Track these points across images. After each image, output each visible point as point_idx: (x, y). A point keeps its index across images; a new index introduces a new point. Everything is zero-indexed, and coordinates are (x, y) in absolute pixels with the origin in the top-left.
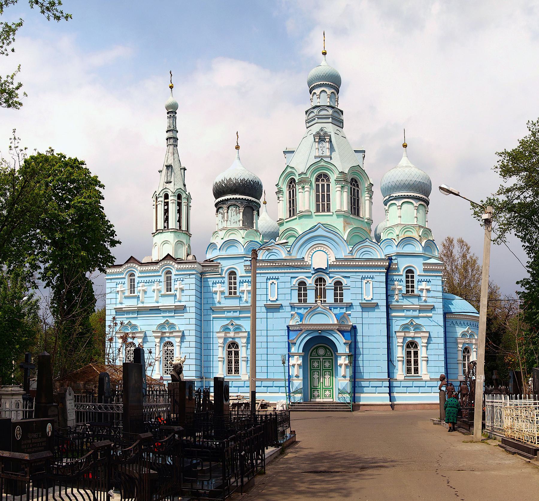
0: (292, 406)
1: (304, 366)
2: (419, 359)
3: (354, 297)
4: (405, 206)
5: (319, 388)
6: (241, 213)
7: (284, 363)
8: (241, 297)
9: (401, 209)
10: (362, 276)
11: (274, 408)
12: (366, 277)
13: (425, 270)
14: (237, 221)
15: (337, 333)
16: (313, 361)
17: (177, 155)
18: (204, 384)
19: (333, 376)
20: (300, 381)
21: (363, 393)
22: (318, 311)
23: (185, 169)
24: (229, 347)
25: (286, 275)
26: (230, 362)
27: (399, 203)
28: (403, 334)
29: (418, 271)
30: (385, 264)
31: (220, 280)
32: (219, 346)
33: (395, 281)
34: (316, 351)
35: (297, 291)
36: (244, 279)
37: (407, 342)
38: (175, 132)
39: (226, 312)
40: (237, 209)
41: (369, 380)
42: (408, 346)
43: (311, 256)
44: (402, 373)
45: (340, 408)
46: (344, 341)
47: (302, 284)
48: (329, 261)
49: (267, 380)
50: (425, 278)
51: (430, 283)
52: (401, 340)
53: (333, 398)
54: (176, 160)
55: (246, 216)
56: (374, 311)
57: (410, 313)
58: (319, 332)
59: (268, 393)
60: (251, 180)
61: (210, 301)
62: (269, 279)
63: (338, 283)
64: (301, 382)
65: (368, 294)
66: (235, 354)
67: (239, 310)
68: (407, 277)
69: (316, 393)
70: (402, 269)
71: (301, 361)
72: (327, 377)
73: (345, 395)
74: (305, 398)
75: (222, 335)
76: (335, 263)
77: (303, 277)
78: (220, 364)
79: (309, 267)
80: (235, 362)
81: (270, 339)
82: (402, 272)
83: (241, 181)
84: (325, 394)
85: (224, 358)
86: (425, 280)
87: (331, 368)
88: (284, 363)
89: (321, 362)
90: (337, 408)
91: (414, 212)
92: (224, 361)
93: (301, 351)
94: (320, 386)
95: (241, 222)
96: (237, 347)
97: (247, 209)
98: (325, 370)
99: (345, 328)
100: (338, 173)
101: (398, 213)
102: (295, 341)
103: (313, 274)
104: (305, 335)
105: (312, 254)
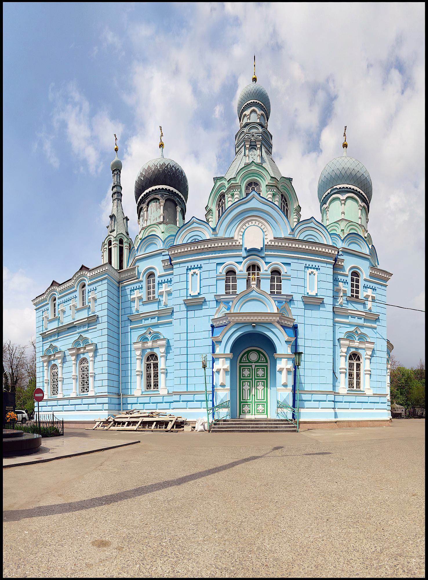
0: (215, 424)
1: (232, 371)
2: (362, 372)
3: (295, 289)
4: (349, 202)
5: (250, 402)
6: (162, 207)
7: (204, 367)
8: (160, 301)
9: (344, 204)
10: (306, 264)
11: (193, 427)
12: (311, 266)
13: (371, 275)
14: (158, 217)
15: (277, 328)
16: (243, 369)
17: (121, 207)
18: (122, 401)
19: (267, 387)
20: (227, 392)
21: (304, 408)
22: (251, 296)
23: (127, 220)
24: (148, 359)
25: (211, 261)
26: (149, 376)
27: (343, 197)
28: (347, 342)
29: (365, 274)
30: (333, 252)
31: (137, 285)
32: (137, 359)
33: (340, 281)
34: (247, 356)
35: (224, 281)
36: (163, 279)
37: (350, 352)
38: (119, 187)
39: (143, 320)
40: (158, 203)
41: (312, 392)
42: (350, 358)
43: (242, 234)
44: (345, 387)
45: (282, 427)
46: (286, 338)
47: (231, 272)
48: (265, 240)
49: (187, 393)
50: (372, 285)
51: (375, 292)
52: (345, 350)
53: (267, 414)
54: (119, 211)
55: (168, 211)
56: (319, 310)
57: (356, 321)
58: (253, 324)
59: (188, 409)
60: (173, 166)
61: (128, 311)
62: (190, 269)
63: (276, 272)
64: (228, 392)
65: (312, 289)
66: (154, 367)
67: (158, 315)
68: (352, 280)
69: (246, 408)
70: (347, 269)
71: (229, 365)
72: (260, 387)
73: (285, 410)
74: (233, 415)
75: (139, 345)
76: (273, 243)
77: (233, 262)
78: (138, 378)
79: (239, 248)
80: (154, 376)
81: (191, 343)
82: (347, 272)
83: (161, 166)
84: (258, 409)
85: (142, 372)
86: (371, 287)
87: (265, 378)
88: (204, 367)
89: (254, 370)
90: (277, 427)
91: (358, 212)
92: (142, 375)
93: (228, 351)
94: (250, 399)
95: (162, 217)
96: (156, 358)
97: (168, 203)
98: (259, 379)
99: (286, 322)
100: (270, 178)
101: (342, 208)
102: (220, 338)
103: (244, 258)
104: (233, 330)
105: (243, 230)
